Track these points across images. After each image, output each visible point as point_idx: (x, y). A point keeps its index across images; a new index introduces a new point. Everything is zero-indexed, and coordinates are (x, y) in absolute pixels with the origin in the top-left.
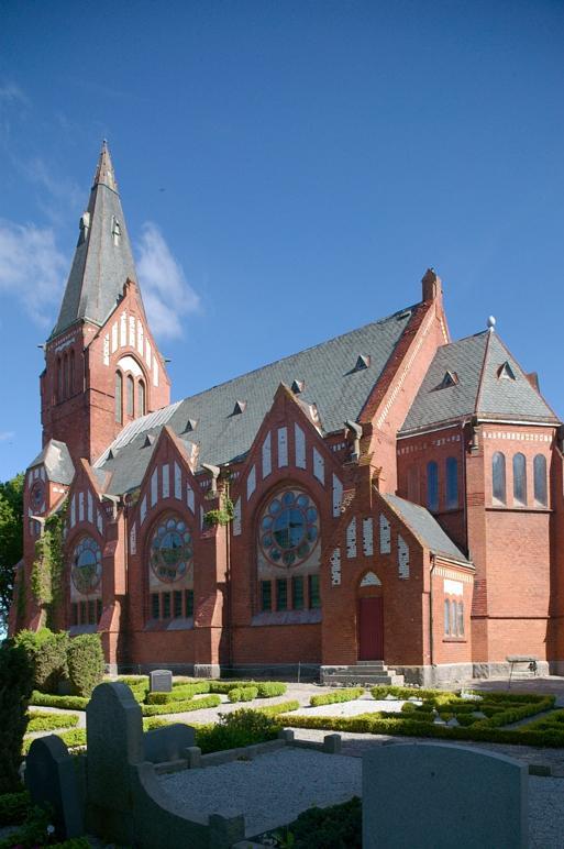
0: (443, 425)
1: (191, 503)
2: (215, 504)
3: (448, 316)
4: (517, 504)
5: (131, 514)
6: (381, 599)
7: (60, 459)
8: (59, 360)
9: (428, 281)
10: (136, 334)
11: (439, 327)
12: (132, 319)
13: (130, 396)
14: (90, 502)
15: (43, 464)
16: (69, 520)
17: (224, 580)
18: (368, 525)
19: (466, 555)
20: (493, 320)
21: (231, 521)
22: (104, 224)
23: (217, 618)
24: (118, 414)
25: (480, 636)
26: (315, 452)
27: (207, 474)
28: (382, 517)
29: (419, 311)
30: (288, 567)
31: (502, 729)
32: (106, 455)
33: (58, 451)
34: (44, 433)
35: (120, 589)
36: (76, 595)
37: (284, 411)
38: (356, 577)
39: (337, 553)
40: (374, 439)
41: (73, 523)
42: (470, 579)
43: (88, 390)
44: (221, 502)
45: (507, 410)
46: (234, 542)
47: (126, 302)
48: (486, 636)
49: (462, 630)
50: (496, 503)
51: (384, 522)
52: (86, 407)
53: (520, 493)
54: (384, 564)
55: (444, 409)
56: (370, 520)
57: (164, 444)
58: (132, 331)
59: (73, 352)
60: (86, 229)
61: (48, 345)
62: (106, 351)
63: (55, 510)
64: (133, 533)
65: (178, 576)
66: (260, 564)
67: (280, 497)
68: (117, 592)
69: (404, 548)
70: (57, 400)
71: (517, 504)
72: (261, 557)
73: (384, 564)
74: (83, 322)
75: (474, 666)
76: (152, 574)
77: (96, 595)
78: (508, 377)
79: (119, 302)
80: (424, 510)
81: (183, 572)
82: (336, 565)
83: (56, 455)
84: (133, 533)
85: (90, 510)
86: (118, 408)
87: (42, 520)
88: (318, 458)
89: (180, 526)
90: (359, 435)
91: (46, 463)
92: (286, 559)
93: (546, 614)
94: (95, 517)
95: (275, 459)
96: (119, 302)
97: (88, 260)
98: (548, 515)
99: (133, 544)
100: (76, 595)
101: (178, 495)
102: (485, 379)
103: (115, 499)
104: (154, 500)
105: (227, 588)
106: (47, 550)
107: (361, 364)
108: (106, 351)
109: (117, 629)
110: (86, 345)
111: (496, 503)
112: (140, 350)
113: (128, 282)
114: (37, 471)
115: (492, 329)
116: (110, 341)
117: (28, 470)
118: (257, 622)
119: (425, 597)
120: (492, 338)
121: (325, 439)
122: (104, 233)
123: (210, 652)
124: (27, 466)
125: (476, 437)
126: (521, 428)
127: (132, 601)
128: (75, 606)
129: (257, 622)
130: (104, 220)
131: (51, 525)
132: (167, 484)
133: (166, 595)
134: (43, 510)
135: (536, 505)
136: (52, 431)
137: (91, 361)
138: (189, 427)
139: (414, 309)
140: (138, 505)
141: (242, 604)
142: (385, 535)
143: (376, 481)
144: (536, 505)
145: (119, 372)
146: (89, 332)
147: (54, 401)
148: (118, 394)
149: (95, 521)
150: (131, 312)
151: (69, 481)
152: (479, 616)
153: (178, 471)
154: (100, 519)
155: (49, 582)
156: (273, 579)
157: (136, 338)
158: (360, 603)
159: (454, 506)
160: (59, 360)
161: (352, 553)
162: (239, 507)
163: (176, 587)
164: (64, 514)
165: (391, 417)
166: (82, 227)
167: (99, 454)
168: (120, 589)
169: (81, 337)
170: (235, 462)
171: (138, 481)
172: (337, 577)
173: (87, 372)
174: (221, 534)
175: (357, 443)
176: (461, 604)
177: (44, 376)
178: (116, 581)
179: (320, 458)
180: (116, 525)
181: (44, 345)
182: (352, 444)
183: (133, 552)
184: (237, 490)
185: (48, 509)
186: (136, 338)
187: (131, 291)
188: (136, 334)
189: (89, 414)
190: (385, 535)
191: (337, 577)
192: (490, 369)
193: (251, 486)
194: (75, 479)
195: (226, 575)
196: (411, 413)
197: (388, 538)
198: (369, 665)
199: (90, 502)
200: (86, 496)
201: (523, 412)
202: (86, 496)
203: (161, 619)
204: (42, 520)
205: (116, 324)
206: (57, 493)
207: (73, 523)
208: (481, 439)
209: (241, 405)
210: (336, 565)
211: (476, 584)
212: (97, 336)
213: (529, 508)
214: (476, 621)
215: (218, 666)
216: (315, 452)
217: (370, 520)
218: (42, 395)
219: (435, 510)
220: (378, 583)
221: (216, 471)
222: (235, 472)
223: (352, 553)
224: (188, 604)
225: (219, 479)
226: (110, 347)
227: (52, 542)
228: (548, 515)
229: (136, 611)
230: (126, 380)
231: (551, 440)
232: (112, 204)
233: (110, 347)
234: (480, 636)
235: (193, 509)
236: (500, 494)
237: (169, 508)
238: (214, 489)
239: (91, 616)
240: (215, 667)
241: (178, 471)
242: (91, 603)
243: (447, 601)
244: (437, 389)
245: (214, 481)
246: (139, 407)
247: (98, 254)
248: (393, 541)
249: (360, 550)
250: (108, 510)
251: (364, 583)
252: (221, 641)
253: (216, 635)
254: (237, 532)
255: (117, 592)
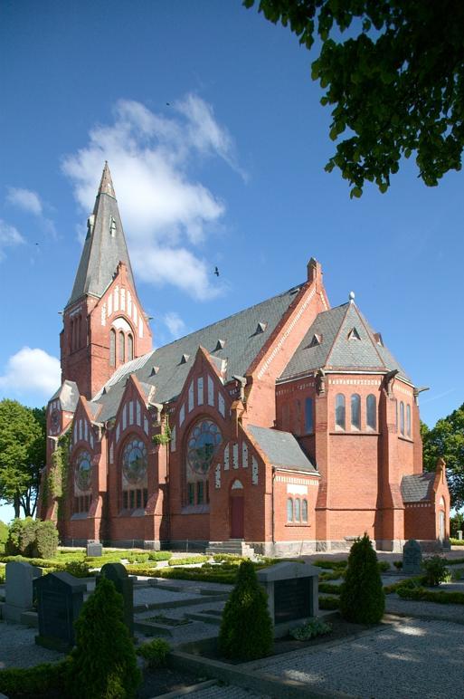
0: (303, 375)
1: (146, 429)
2: (158, 430)
3: (327, 286)
4: (354, 429)
5: (110, 436)
6: (243, 498)
7: (71, 394)
8: (72, 322)
9: (311, 266)
10: (126, 301)
11: (319, 299)
12: (123, 291)
13: (122, 346)
14: (86, 426)
15: (58, 398)
16: (73, 439)
17: (164, 482)
18: (236, 448)
19: (314, 464)
20: (353, 295)
21: (170, 441)
22: (104, 223)
23: (98, 513)
24: (112, 360)
25: (321, 522)
26: (220, 395)
27: (155, 409)
28: (244, 444)
29: (304, 287)
30: (205, 474)
31: (327, 583)
32: (102, 391)
33: (70, 388)
34: (62, 375)
35: (103, 487)
36: (78, 492)
37: (201, 368)
38: (229, 482)
39: (219, 467)
40: (254, 387)
41: (76, 441)
42: (317, 483)
43: (90, 345)
44: (163, 429)
45: (348, 362)
46: (171, 455)
47: (119, 277)
48: (325, 522)
49: (306, 518)
50: (338, 429)
51: (245, 447)
52: (89, 357)
53: (357, 422)
54: (244, 474)
55: (305, 366)
56: (237, 445)
57: (200, 359)
58: (123, 299)
59: (80, 317)
60: (92, 227)
61: (65, 312)
62: (103, 316)
63: (65, 432)
64: (112, 448)
65: (140, 479)
66: (188, 472)
67: (199, 425)
68: (100, 490)
69: (255, 465)
70: (71, 350)
71: (354, 429)
72: (188, 467)
73: (244, 474)
74: (87, 296)
75: (317, 543)
76: (123, 478)
77: (89, 493)
78: (356, 338)
79: (114, 278)
80: (289, 435)
81: (142, 477)
82: (218, 474)
83: (68, 393)
84: (112, 448)
85: (139, 416)
86: (113, 356)
87: (56, 439)
88: (221, 399)
89: (141, 444)
90: (244, 384)
91: (61, 398)
92: (203, 468)
93: (375, 507)
94: (89, 437)
95: (128, 422)
96: (114, 278)
97: (92, 250)
98: (377, 437)
99: (112, 457)
100: (78, 492)
101: (211, 402)
102: (338, 340)
103: (100, 425)
104: (125, 426)
105: (166, 488)
106: (59, 460)
107: (259, 329)
108: (103, 316)
109: (100, 516)
110: (89, 311)
111: (338, 429)
112: (129, 313)
113: (120, 264)
114: (55, 403)
115: (352, 301)
116: (107, 308)
117: (50, 402)
118: (185, 512)
119: (267, 498)
120: (351, 308)
121: (225, 386)
122: (104, 229)
123: (153, 532)
124: (48, 400)
125: (323, 384)
126: (358, 376)
127: (111, 496)
128: (77, 498)
129: (185, 512)
130: (105, 220)
131: (62, 442)
132: (132, 417)
133: (132, 492)
134: (58, 431)
135: (369, 429)
136: (67, 375)
137: (92, 323)
138: (219, 347)
139: (301, 286)
140: (114, 429)
141: (176, 499)
142: (245, 456)
143: (240, 420)
144: (369, 429)
145: (113, 330)
146: (91, 303)
147: (68, 352)
148: (112, 345)
149: (89, 439)
150: (123, 286)
151: (73, 410)
152: (321, 509)
153: (138, 406)
154: (92, 438)
155: (60, 482)
156: (195, 482)
157: (126, 304)
158: (231, 500)
159: (310, 432)
160: (72, 322)
161: (227, 467)
162: (174, 432)
163: (138, 487)
164: (70, 435)
165: (272, 369)
166: (89, 226)
167: (98, 390)
168: (103, 487)
169: (85, 307)
170: (173, 401)
171: (114, 413)
172: (218, 482)
173: (89, 332)
174: (162, 452)
175: (242, 390)
176: (305, 501)
177: (62, 334)
178: (100, 483)
179: (223, 399)
180: (100, 443)
181: (62, 311)
182: (239, 391)
183: (112, 462)
184: (173, 421)
185: (62, 430)
186: (126, 304)
187: (123, 271)
188: (126, 301)
189: (91, 362)
190: (245, 456)
191: (218, 482)
192: (344, 332)
193: (182, 418)
194: (77, 410)
195: (166, 478)
196: (289, 365)
197: (247, 457)
198: (235, 541)
199: (86, 426)
200: (83, 422)
201: (361, 364)
202: (83, 422)
203: (129, 509)
204: (56, 439)
205: (111, 295)
206: (68, 418)
207: (76, 441)
208: (327, 385)
209: (222, 342)
210: (218, 474)
211: (321, 486)
212: (97, 306)
213: (363, 432)
214: (319, 512)
215: (159, 541)
216: (220, 395)
217: (237, 445)
218: (61, 347)
219: (299, 433)
220: (242, 487)
221: (160, 407)
222: (172, 407)
223: (227, 467)
224: (143, 498)
225: (163, 412)
226: (106, 312)
227: (62, 454)
228: (377, 437)
229: (113, 502)
230: (119, 336)
231: (380, 383)
232: (111, 207)
233: (106, 312)
234: (321, 522)
235: (223, 413)
236: (341, 422)
237: (132, 433)
238: (159, 419)
239: (139, 502)
240: (157, 542)
241: (138, 406)
242: (86, 497)
243: (291, 499)
244: (308, 347)
245: (159, 414)
246: (128, 354)
247: (100, 244)
248: (250, 460)
249: (232, 465)
250: (153, 416)
251: (234, 487)
252: (161, 525)
253: (158, 520)
254: (173, 449)
255: (100, 490)
